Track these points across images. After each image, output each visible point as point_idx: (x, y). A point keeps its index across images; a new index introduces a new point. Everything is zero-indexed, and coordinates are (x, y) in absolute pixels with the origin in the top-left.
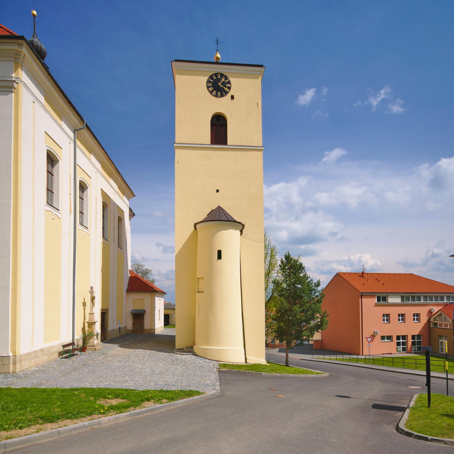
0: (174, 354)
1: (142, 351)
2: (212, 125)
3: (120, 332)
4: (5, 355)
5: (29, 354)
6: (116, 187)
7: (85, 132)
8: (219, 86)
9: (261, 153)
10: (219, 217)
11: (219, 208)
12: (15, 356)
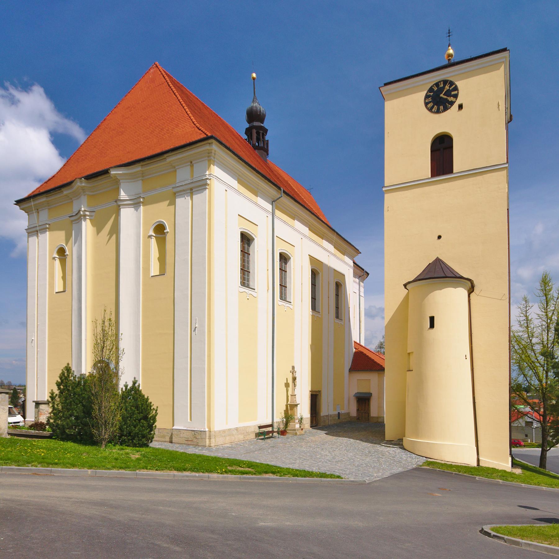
0: (378, 446)
1: (345, 440)
2: (432, 151)
3: (339, 418)
4: (202, 430)
5: (224, 431)
6: (330, 247)
7: (286, 200)
8: (441, 97)
9: (504, 172)
10: (438, 273)
11: (438, 261)
12: (210, 431)
